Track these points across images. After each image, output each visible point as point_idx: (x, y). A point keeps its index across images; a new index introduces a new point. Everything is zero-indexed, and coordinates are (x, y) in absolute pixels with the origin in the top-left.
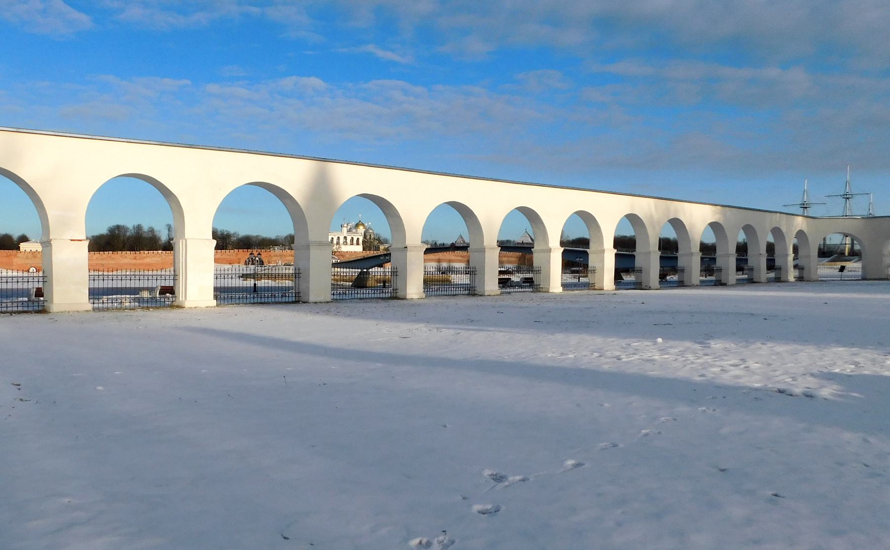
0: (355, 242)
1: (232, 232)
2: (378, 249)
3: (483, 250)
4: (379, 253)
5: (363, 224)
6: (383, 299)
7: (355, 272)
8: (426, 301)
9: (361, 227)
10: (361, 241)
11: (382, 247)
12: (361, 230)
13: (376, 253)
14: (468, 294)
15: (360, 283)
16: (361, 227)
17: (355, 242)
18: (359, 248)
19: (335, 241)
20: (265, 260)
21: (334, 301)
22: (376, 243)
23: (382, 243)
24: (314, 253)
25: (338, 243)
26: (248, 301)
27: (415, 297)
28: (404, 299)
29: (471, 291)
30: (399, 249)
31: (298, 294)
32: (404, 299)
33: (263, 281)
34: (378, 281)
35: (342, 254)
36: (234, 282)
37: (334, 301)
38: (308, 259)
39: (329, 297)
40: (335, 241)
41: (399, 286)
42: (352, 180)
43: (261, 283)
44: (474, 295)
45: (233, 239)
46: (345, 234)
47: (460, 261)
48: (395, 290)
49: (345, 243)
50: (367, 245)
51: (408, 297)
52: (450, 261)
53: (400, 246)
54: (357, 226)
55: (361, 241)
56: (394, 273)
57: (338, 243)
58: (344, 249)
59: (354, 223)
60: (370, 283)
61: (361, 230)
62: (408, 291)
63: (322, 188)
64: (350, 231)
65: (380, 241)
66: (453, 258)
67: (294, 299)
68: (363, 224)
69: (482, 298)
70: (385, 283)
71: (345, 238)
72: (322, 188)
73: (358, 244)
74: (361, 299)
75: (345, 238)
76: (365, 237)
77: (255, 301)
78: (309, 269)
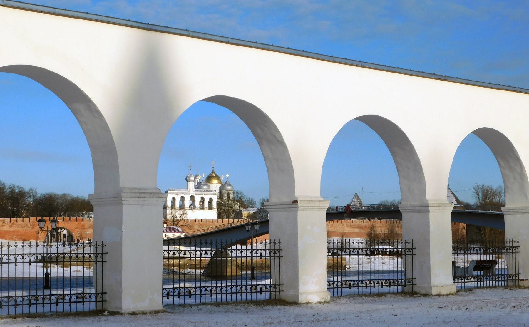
0: (206, 205)
1: (27, 189)
2: (239, 215)
3: (424, 209)
4: (242, 222)
5: (217, 177)
6: (257, 303)
7: (206, 254)
8: (334, 307)
9: (215, 181)
10: (215, 204)
11: (245, 213)
12: (215, 185)
13: (236, 222)
14: (403, 293)
15: (215, 270)
16: (215, 181)
17: (206, 205)
18: (212, 215)
19: (178, 204)
20: (76, 235)
21: (169, 308)
22: (237, 206)
23: (245, 207)
24: (130, 211)
25: (182, 207)
26: (19, 310)
27: (315, 299)
28: (295, 303)
29: (407, 286)
30: (281, 206)
31: (100, 296)
32: (295, 303)
33: (74, 268)
34: (242, 267)
35: (188, 224)
36: (26, 270)
37: (169, 308)
38: (119, 224)
39: (157, 301)
40: (178, 204)
41: (285, 279)
42: (206, 69)
43: (56, 271)
44: (413, 294)
45: (29, 200)
46: (192, 192)
47: (358, 235)
48: (277, 285)
49: (192, 206)
50: (224, 210)
51: (302, 299)
52: (343, 234)
53: (286, 199)
54: (209, 179)
55: (215, 204)
56: (276, 251)
57: (182, 207)
58: (192, 215)
59: (204, 176)
60: (230, 270)
61: (215, 185)
62: (302, 288)
63: (149, 83)
64: (198, 187)
65: (244, 204)
66: (347, 230)
67: (93, 306)
68: (217, 177)
69: (427, 300)
70: (255, 270)
71: (192, 198)
72: (149, 83)
73: (210, 208)
74: (217, 304)
75: (192, 198)
76: (221, 196)
77: (33, 309)
78: (120, 244)
